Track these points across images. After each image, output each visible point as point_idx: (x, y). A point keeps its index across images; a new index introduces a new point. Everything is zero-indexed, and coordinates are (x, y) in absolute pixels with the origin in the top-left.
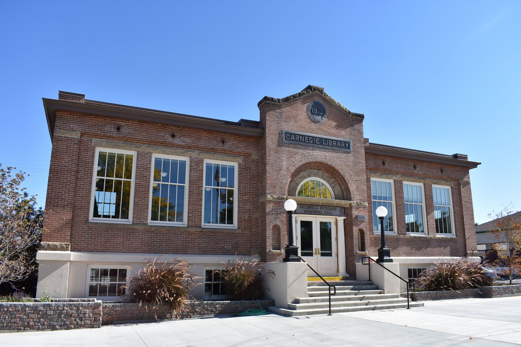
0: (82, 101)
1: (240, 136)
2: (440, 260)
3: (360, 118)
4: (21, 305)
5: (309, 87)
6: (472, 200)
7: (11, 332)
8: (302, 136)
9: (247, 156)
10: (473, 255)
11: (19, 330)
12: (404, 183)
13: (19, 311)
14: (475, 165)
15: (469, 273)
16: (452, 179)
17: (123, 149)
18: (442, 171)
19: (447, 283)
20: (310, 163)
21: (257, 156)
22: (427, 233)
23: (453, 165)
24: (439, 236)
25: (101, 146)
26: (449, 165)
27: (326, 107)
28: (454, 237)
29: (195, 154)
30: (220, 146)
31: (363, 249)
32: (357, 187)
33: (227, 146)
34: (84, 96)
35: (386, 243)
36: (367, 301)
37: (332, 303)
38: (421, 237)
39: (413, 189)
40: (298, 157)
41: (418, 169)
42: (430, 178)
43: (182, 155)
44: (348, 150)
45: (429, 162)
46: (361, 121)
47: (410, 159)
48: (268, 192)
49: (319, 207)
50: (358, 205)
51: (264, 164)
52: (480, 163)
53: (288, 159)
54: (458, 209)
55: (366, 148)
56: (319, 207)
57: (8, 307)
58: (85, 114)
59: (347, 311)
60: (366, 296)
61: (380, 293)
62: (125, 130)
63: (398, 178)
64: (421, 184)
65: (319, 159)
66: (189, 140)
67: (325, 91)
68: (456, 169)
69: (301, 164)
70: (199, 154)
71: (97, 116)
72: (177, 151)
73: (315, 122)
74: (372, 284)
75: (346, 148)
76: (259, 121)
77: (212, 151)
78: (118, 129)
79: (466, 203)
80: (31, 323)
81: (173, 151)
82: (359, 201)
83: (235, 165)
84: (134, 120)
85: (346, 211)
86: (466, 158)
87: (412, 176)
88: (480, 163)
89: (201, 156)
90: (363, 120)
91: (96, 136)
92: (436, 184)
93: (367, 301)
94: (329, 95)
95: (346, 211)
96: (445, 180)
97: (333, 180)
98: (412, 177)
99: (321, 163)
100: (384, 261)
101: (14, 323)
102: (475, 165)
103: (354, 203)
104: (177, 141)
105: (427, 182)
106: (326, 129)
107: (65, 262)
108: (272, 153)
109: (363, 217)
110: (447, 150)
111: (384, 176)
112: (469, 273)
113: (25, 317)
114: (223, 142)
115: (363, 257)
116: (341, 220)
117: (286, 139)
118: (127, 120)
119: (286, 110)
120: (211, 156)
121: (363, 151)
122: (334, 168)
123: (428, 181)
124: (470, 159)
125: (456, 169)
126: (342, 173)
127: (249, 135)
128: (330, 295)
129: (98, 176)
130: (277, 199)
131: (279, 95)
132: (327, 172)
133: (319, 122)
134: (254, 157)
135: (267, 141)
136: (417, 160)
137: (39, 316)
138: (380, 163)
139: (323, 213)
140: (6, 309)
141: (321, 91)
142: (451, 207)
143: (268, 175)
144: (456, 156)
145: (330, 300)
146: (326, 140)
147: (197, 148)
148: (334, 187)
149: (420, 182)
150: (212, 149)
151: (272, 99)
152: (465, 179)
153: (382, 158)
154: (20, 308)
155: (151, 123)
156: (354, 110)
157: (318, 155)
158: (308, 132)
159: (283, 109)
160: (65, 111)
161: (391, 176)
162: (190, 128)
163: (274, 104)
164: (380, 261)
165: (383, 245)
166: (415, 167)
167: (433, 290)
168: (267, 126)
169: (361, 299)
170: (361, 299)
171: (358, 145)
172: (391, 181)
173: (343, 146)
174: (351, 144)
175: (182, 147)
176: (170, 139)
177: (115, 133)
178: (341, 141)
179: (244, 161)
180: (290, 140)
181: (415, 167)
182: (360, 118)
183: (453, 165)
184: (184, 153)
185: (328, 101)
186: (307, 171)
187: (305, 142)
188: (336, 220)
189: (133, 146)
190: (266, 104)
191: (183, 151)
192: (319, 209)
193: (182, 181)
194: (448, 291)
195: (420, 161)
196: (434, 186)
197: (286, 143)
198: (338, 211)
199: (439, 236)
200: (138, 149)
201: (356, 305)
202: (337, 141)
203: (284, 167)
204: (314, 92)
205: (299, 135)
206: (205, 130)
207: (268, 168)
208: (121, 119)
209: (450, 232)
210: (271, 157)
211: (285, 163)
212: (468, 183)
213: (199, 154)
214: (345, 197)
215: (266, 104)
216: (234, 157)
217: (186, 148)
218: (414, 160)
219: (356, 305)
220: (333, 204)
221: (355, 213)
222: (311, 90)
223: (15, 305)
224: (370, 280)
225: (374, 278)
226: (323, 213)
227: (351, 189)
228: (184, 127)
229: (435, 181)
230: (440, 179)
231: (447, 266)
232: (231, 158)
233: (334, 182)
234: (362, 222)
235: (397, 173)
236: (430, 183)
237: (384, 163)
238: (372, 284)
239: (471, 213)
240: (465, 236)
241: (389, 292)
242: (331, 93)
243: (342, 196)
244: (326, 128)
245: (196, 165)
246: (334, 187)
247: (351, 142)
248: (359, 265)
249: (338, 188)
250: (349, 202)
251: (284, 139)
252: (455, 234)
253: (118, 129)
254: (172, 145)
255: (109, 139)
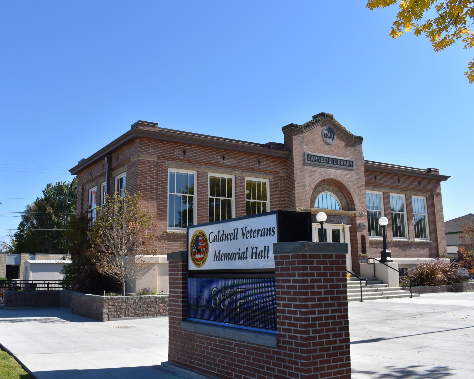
0: (156, 129)
1: (271, 157)
2: (422, 260)
3: (360, 139)
4: (154, 297)
5: (322, 114)
6: (442, 209)
7: (148, 318)
8: (319, 157)
9: (276, 173)
10: (443, 257)
11: (154, 316)
12: (391, 194)
13: (152, 302)
14: (445, 178)
15: (445, 272)
16: (427, 191)
17: (188, 169)
18: (419, 184)
19: (428, 279)
20: (325, 180)
21: (284, 174)
22: (408, 238)
23: (428, 179)
24: (417, 240)
25: (172, 167)
26: (425, 178)
27: (335, 131)
28: (429, 241)
29: (238, 173)
30: (256, 166)
31: (364, 251)
32: (359, 200)
33: (262, 166)
34: (157, 124)
35: (388, 246)
36: (381, 292)
37: (363, 293)
38: (404, 242)
39: (397, 200)
40: (317, 175)
41: (401, 182)
42: (410, 190)
43: (230, 173)
44: (352, 168)
45: (410, 176)
46: (361, 143)
47: (395, 174)
48: (296, 205)
49: (332, 217)
50: (360, 215)
51: (293, 182)
52: (450, 177)
53: (310, 176)
54: (431, 216)
55: (365, 166)
56: (332, 217)
57: (145, 299)
58: (160, 141)
59: (370, 299)
60: (379, 288)
61: (386, 287)
62: (189, 154)
63: (385, 190)
64: (403, 196)
65: (331, 177)
66: (235, 162)
67: (334, 117)
68: (428, 182)
69: (319, 180)
70: (242, 173)
71: (168, 142)
72: (226, 170)
73: (328, 144)
74: (377, 280)
75: (350, 166)
76: (283, 143)
77: (251, 170)
78: (184, 153)
79: (438, 212)
80: (161, 311)
81: (223, 170)
82: (361, 212)
83: (267, 181)
84: (194, 145)
85: (352, 221)
86: (438, 172)
87: (396, 189)
88: (450, 177)
89: (244, 174)
90: (362, 141)
91: (168, 159)
92: (415, 195)
93: (381, 292)
94: (337, 121)
95: (352, 221)
96: (421, 191)
97: (340, 193)
98: (397, 189)
99: (332, 180)
100: (387, 261)
101: (150, 311)
102: (445, 178)
103: (357, 212)
104: (226, 162)
105: (408, 194)
106: (336, 151)
107: (153, 264)
108: (298, 172)
109: (364, 225)
110: (421, 164)
111: (376, 189)
112: (445, 272)
113: (157, 306)
114: (259, 162)
115: (364, 258)
116: (347, 227)
117: (308, 160)
118: (190, 145)
119: (307, 134)
120: (251, 174)
121: (362, 169)
122: (342, 184)
123: (409, 193)
124: (441, 173)
125: (428, 182)
126: (348, 188)
127: (278, 156)
128: (361, 287)
129: (193, 197)
130: (304, 210)
131: (300, 122)
132: (336, 187)
133: (330, 144)
134: (282, 175)
135: (295, 162)
136: (400, 175)
137: (166, 305)
138: (373, 178)
139: (335, 222)
140: (144, 300)
141: (331, 117)
142: (426, 215)
143: (296, 191)
144: (430, 170)
145: (361, 291)
146: (336, 160)
147: (240, 168)
148: (341, 199)
149: (402, 194)
150: (251, 168)
151: (297, 125)
152: (438, 191)
153: (380, 175)
154: (153, 300)
155: (207, 147)
156: (355, 133)
157: (331, 173)
158: (322, 153)
159: (304, 134)
160: (145, 138)
161: (381, 189)
162: (235, 151)
163: (298, 130)
164: (383, 261)
165: (385, 248)
166: (399, 181)
167: (418, 286)
168: (294, 149)
169: (376, 291)
170: (376, 291)
171: (360, 164)
172: (380, 193)
173: (348, 165)
174: (354, 163)
175: (229, 167)
176: (221, 161)
177: (182, 156)
178: (347, 161)
179: (274, 178)
180: (310, 161)
181: (399, 181)
182: (360, 139)
183: (428, 179)
184: (231, 172)
185: (337, 126)
186: (322, 186)
187: (321, 162)
188: (344, 227)
189: (195, 166)
190: (290, 130)
191: (230, 171)
192: (332, 219)
193: (230, 196)
194: (430, 287)
195: (403, 175)
196: (413, 197)
197: (307, 164)
198: (345, 220)
199: (417, 240)
200: (198, 170)
201: (373, 295)
202: (344, 161)
203: (307, 184)
204: (327, 119)
205: (317, 156)
206: (246, 153)
207: (296, 185)
208: (186, 144)
209: (425, 237)
210: (297, 176)
211: (307, 181)
212: (439, 194)
213: (242, 173)
214: (350, 208)
215: (290, 130)
216: (267, 174)
217: (233, 168)
218: (398, 174)
219: (373, 295)
220: (342, 214)
221: (358, 221)
222: (324, 116)
223: (150, 297)
224: (375, 277)
225: (378, 275)
226: (335, 222)
227: (355, 201)
228: (231, 150)
229: (414, 192)
230: (417, 191)
231: (427, 266)
232: (265, 175)
233: (341, 195)
234: (364, 229)
235: (385, 186)
236: (410, 194)
237: (376, 178)
238: (377, 280)
239: (442, 221)
240: (437, 241)
241: (391, 286)
242: (340, 119)
243: (347, 207)
244: (337, 150)
245: (240, 180)
246: (341, 199)
247: (354, 161)
248: (363, 264)
249: (344, 200)
250: (354, 212)
251: (306, 160)
252: (429, 238)
253: (184, 153)
254: (222, 166)
255: (179, 162)
